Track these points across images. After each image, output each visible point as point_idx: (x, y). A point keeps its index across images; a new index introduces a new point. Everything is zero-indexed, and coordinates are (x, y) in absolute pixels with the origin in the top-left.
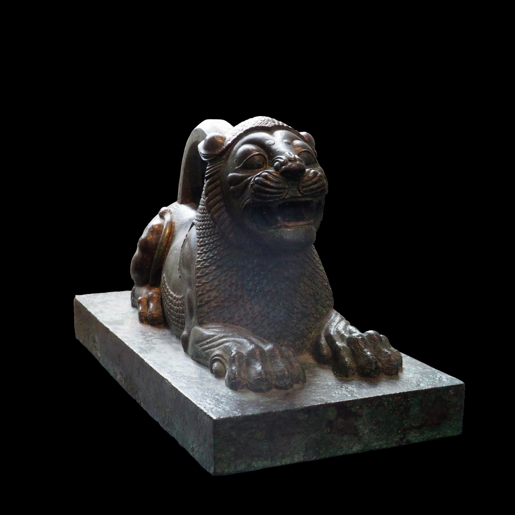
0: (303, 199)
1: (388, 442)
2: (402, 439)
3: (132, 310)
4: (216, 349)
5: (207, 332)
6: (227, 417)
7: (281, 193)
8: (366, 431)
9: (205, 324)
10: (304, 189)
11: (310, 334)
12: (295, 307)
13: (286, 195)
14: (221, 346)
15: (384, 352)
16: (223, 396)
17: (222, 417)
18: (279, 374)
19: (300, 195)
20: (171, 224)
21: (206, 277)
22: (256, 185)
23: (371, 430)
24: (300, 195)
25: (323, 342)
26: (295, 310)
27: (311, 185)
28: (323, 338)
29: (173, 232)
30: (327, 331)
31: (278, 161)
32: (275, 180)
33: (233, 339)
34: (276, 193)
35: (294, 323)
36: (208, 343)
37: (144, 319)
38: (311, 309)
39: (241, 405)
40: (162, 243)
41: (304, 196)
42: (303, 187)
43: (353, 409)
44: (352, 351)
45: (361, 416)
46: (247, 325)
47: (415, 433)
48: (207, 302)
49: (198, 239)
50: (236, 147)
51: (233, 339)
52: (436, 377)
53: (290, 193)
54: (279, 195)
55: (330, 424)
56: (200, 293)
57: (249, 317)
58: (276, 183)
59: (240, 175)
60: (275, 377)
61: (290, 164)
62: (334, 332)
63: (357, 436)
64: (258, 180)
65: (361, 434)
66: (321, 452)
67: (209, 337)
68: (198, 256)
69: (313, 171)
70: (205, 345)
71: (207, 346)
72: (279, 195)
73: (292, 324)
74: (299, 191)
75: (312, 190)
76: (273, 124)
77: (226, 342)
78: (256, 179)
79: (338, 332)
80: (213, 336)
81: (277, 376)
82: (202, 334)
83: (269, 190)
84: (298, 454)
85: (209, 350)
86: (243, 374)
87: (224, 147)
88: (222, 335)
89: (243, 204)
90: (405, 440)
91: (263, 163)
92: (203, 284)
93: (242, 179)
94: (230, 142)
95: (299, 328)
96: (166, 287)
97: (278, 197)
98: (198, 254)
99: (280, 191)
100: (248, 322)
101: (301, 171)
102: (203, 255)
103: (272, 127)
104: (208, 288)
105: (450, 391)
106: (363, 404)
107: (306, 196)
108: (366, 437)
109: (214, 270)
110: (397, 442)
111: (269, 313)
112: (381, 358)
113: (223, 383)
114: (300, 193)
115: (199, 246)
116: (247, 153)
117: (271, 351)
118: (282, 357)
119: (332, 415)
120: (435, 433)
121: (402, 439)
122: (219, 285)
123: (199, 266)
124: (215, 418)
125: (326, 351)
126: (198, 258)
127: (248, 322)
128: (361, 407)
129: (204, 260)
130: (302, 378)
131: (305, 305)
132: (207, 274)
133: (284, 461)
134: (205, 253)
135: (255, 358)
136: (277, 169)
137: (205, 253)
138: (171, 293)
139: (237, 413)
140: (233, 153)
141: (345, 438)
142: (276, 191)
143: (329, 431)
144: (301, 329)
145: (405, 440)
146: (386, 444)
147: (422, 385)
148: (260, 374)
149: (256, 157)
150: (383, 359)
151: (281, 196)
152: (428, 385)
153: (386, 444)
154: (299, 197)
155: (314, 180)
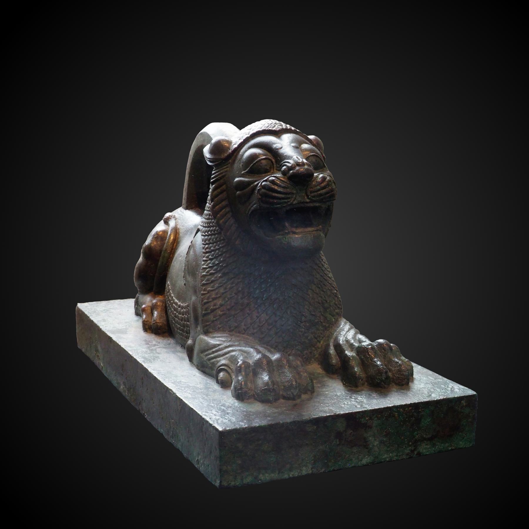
0: (311, 205)
1: (399, 454)
2: (413, 451)
3: (135, 318)
4: (221, 358)
5: (212, 342)
6: (233, 428)
7: (289, 198)
8: (376, 443)
9: (211, 332)
10: (312, 194)
11: (318, 343)
12: (303, 315)
13: (294, 200)
14: (227, 355)
15: (394, 361)
16: (229, 407)
17: (228, 429)
18: (286, 384)
19: (308, 200)
20: (176, 231)
21: (212, 285)
22: (263, 190)
23: (381, 442)
24: (308, 200)
25: (332, 351)
26: (303, 318)
27: (319, 190)
28: (332, 348)
29: (178, 238)
30: (336, 340)
31: (286, 165)
32: (282, 185)
33: (239, 348)
34: (283, 199)
35: (302, 332)
36: (213, 352)
37: (148, 328)
38: (320, 317)
39: (247, 416)
40: (166, 250)
41: (312, 201)
42: (311, 192)
43: (363, 421)
44: (362, 360)
45: (370, 427)
46: (253, 334)
47: (426, 445)
48: (213, 311)
49: (203, 246)
50: (242, 151)
51: (239, 348)
52: (448, 387)
53: (298, 198)
54: (286, 201)
55: (339, 435)
56: (205, 301)
57: (256, 326)
58: (284, 187)
59: (246, 179)
60: (282, 387)
61: (297, 168)
62: (343, 341)
63: (367, 448)
64: (265, 185)
65: (371, 446)
66: (330, 464)
67: (215, 346)
68: (203, 263)
69: (321, 175)
70: (210, 354)
71: (212, 355)
72: (286, 201)
73: (300, 333)
74: (308, 196)
75: (321, 195)
76: (281, 127)
77: (233, 351)
78: (263, 183)
79: (347, 341)
80: (219, 345)
81: (284, 386)
82: (208, 343)
83: (276, 195)
84: (306, 466)
85: (214, 360)
86: (249, 385)
87: (230, 151)
88: (228, 344)
89: (250, 210)
90: (416, 452)
91: (270, 168)
92: (209, 292)
93: (249, 183)
94: (236, 146)
95: (307, 337)
96: (170, 295)
97: (285, 202)
98: (204, 261)
99: (288, 196)
100: (255, 331)
101: (309, 176)
102: (209, 262)
103: (279, 130)
104: (214, 296)
105: (462, 402)
106: (373, 415)
107: (314, 201)
108: (376, 449)
109: (220, 277)
110: (407, 454)
111: (276, 322)
112: (391, 368)
113: (229, 393)
114: (308, 198)
115: (204, 253)
116: (253, 157)
117: (279, 360)
118: (290, 366)
119: (341, 426)
120: (447, 445)
121: (413, 451)
122: (225, 293)
123: (205, 273)
124: (220, 429)
125: (335, 361)
126: (203, 265)
127: (255, 331)
128: (371, 418)
129: (210, 267)
130: (310, 388)
131: (313, 313)
132: (212, 282)
133: (292, 473)
134: (211, 259)
135: (262, 368)
136: (284, 173)
137: (211, 259)
138: (176, 301)
139: (244, 425)
140: (239, 157)
141: (355, 450)
142: (283, 196)
143: (338, 443)
144: (309, 338)
145: (416, 452)
146: (397, 456)
147: (433, 395)
148: (267, 384)
149: (263, 161)
150: (393, 369)
151: (288, 202)
152: (440, 396)
153: (397, 456)
154: (307, 203)
155: (323, 185)
